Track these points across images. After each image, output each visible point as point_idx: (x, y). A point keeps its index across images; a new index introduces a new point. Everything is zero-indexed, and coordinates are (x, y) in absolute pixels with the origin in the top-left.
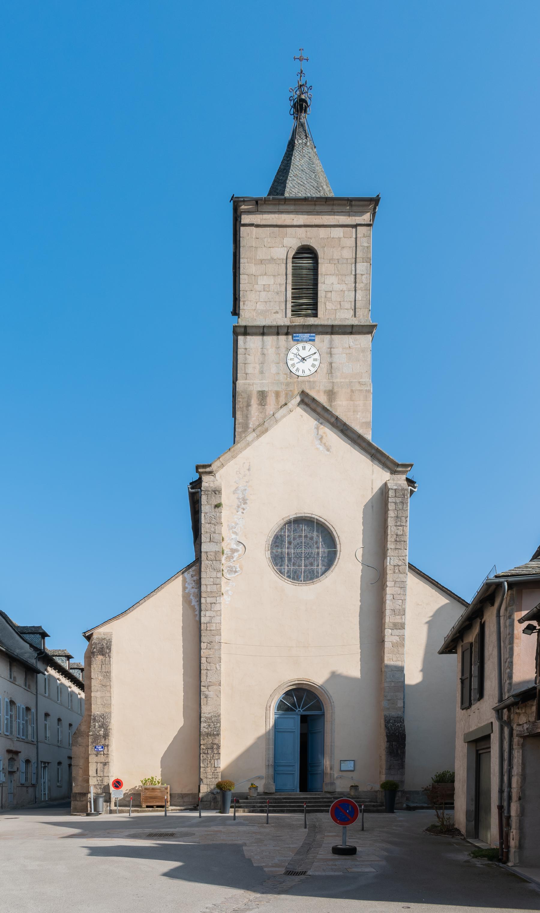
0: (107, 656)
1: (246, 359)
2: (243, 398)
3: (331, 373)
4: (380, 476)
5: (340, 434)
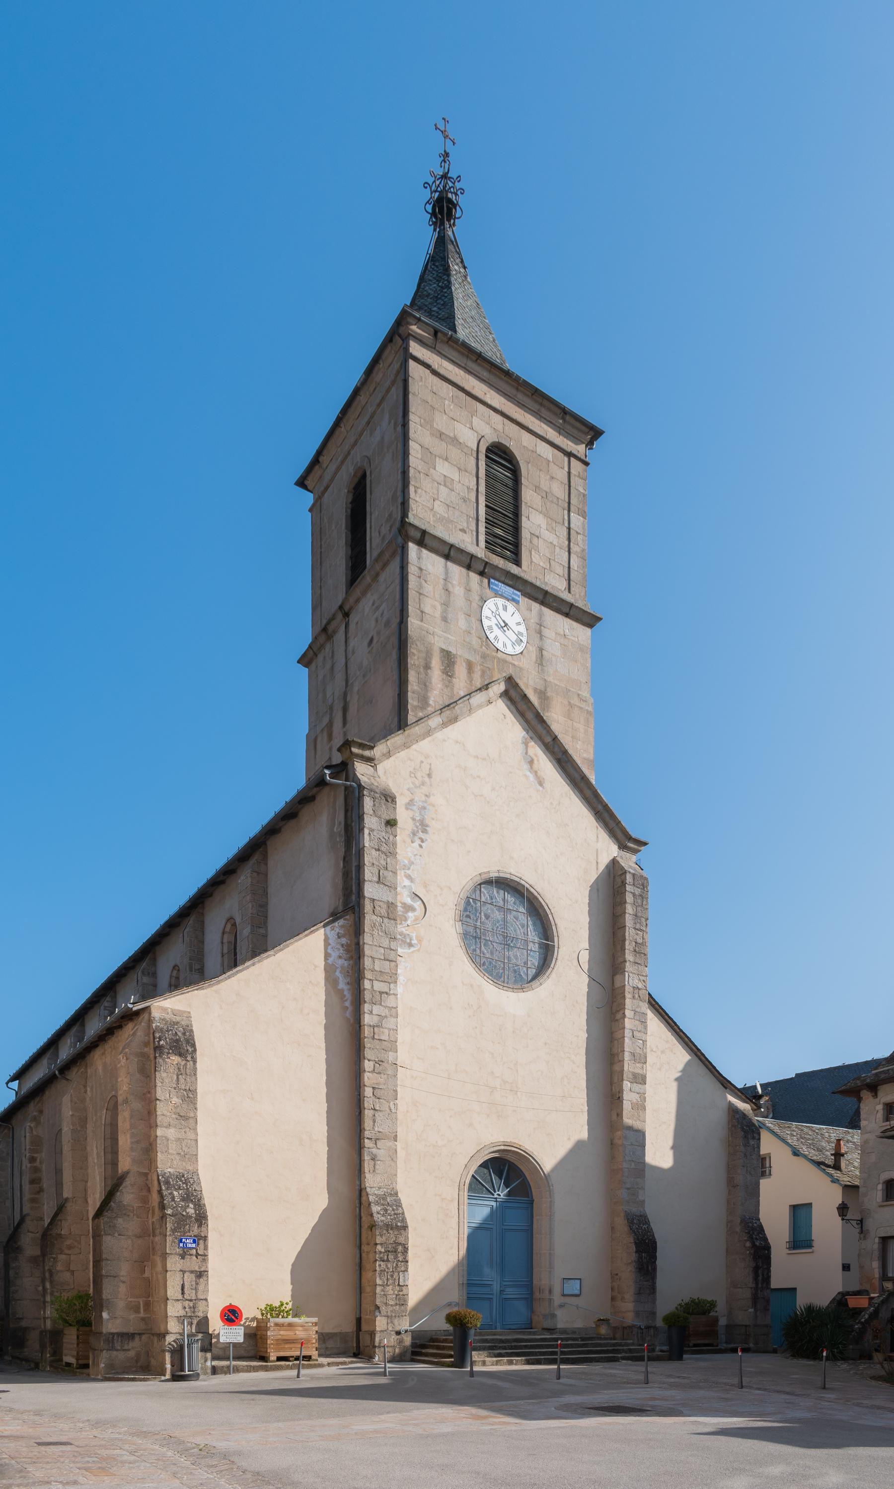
0: (189, 1058)
1: (420, 586)
4: (609, 850)
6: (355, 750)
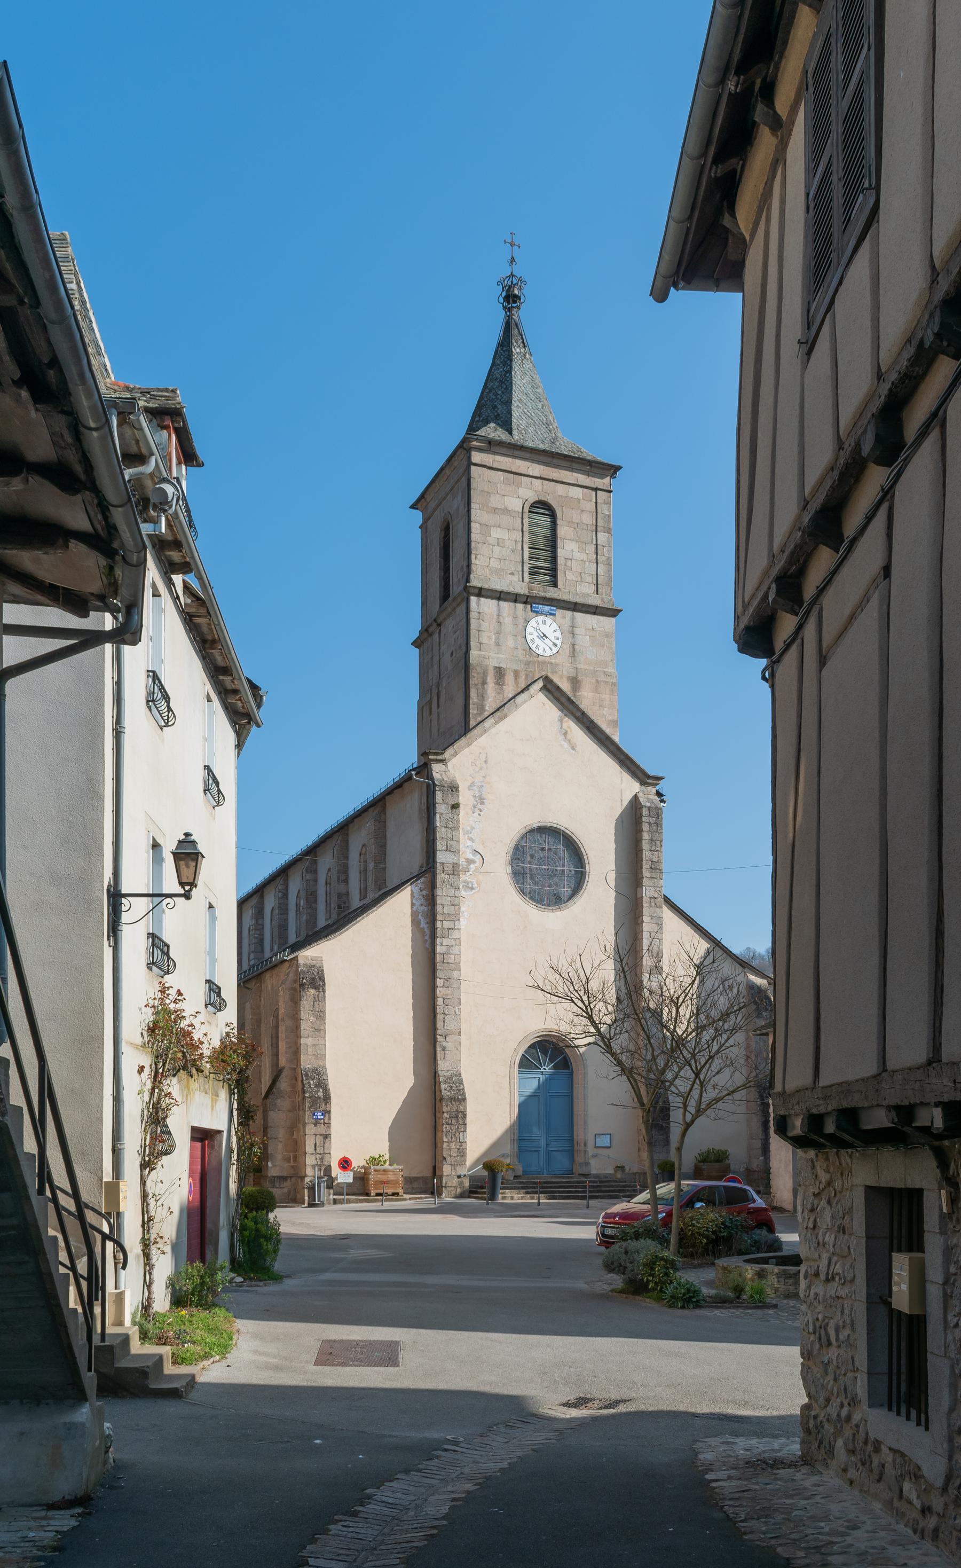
1: (480, 625)
2: (478, 673)
4: (631, 787)
6: (431, 757)
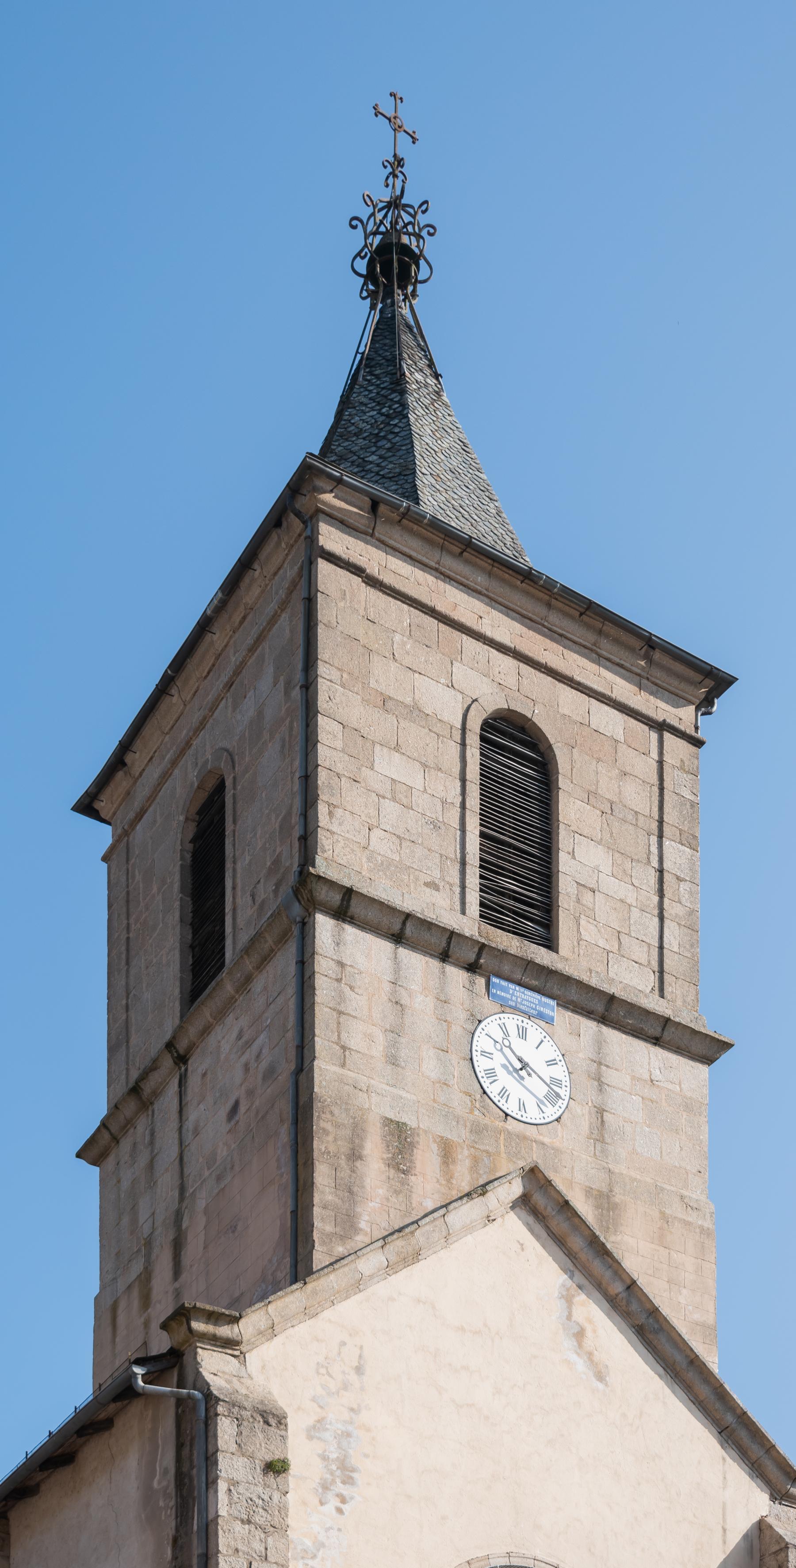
1: (341, 998)
2: (337, 1126)
3: (601, 1140)
4: (749, 1502)
5: (634, 1338)
6: (198, 1326)
